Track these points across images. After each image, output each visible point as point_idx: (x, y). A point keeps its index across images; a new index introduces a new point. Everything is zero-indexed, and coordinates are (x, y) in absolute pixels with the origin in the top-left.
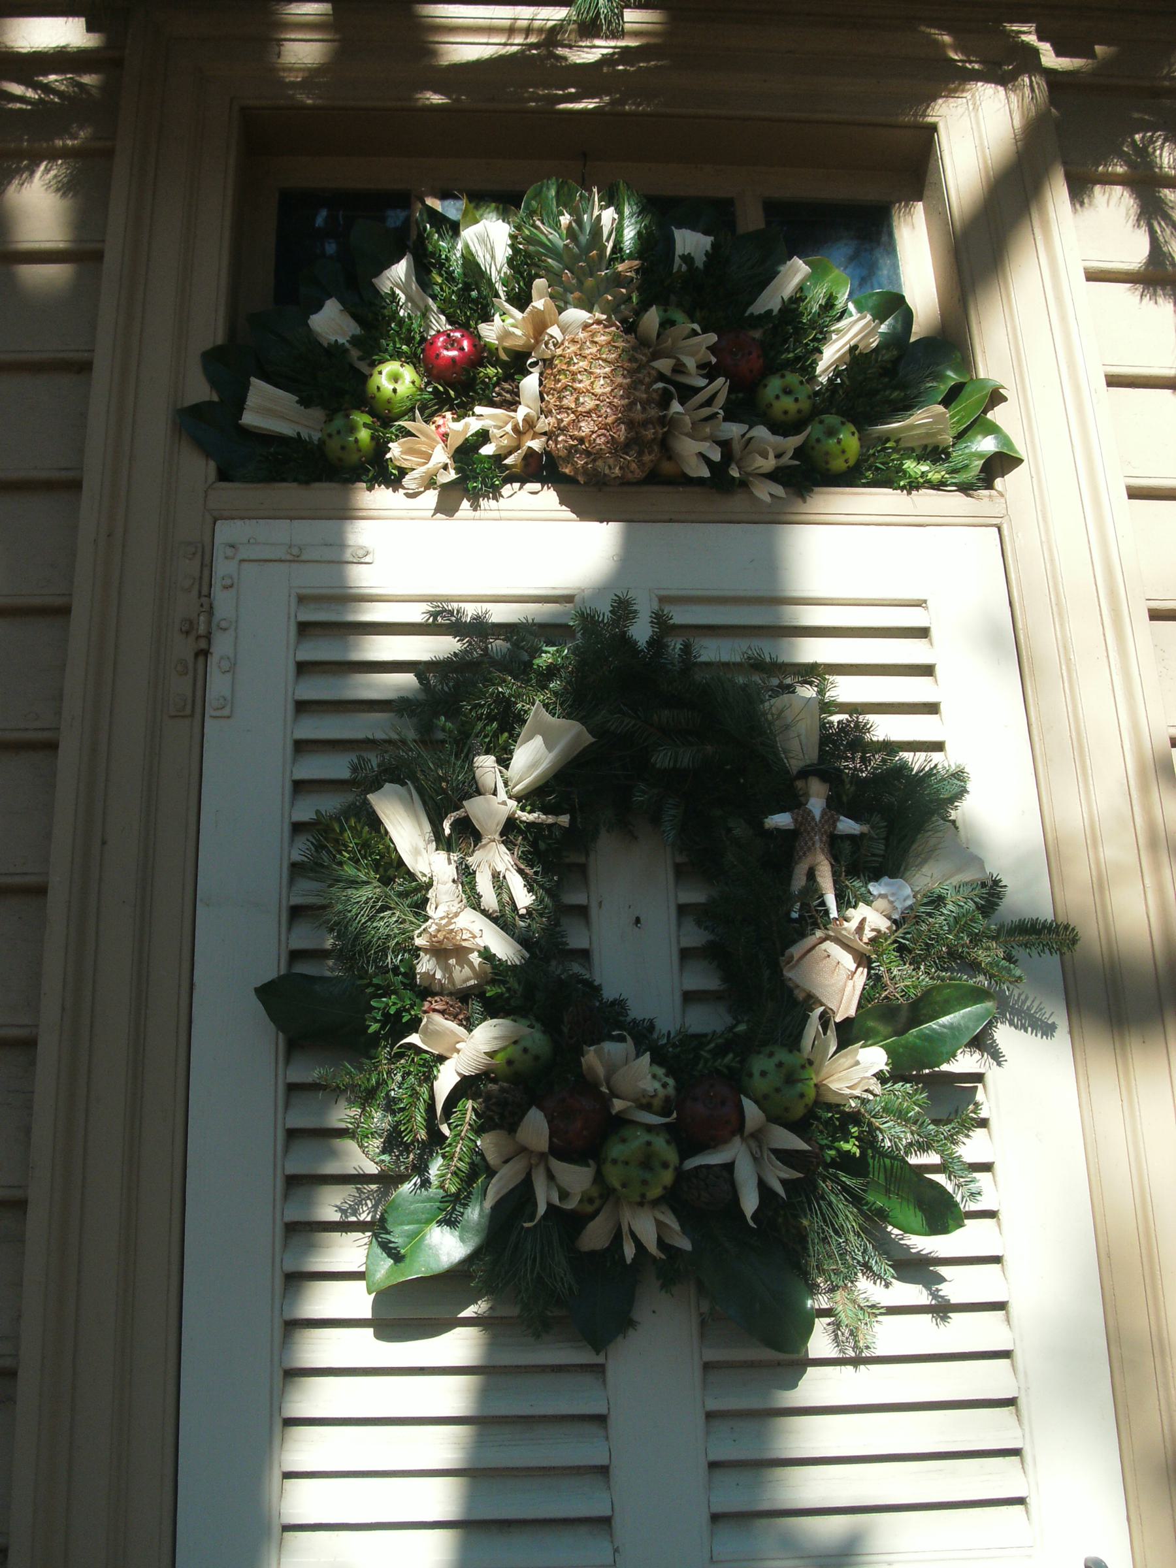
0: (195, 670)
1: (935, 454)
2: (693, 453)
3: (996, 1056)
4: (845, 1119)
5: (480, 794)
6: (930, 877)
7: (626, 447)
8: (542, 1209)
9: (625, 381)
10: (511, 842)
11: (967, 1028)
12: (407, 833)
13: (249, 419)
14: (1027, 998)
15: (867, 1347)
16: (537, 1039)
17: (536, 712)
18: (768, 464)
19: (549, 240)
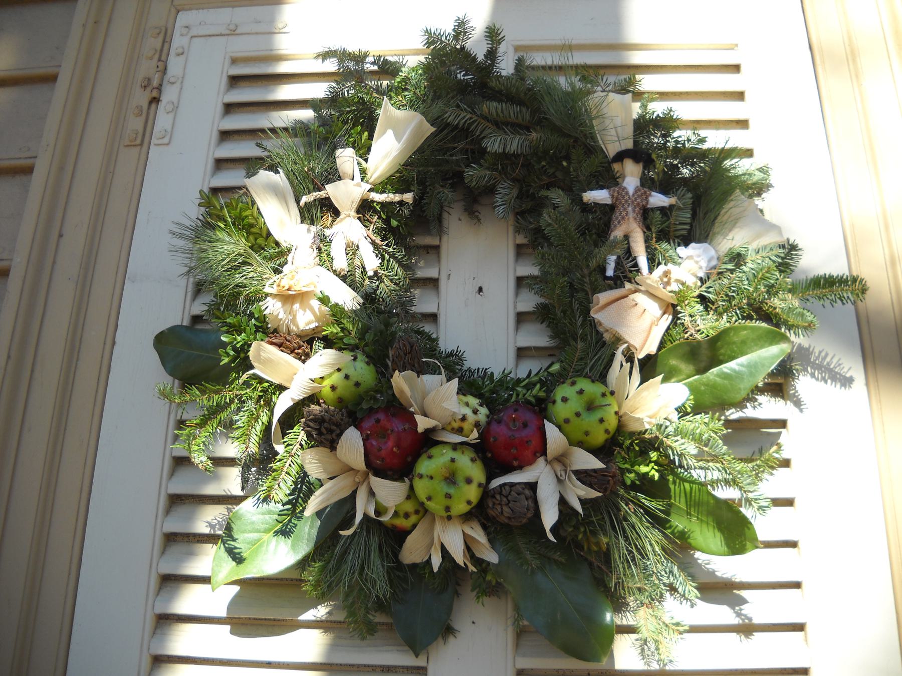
0: (148, 114)
3: (798, 403)
4: (647, 445)
6: (735, 239)
8: (359, 518)
10: (368, 220)
11: (763, 365)
12: (280, 217)
14: (827, 355)
15: (671, 661)
16: (363, 371)
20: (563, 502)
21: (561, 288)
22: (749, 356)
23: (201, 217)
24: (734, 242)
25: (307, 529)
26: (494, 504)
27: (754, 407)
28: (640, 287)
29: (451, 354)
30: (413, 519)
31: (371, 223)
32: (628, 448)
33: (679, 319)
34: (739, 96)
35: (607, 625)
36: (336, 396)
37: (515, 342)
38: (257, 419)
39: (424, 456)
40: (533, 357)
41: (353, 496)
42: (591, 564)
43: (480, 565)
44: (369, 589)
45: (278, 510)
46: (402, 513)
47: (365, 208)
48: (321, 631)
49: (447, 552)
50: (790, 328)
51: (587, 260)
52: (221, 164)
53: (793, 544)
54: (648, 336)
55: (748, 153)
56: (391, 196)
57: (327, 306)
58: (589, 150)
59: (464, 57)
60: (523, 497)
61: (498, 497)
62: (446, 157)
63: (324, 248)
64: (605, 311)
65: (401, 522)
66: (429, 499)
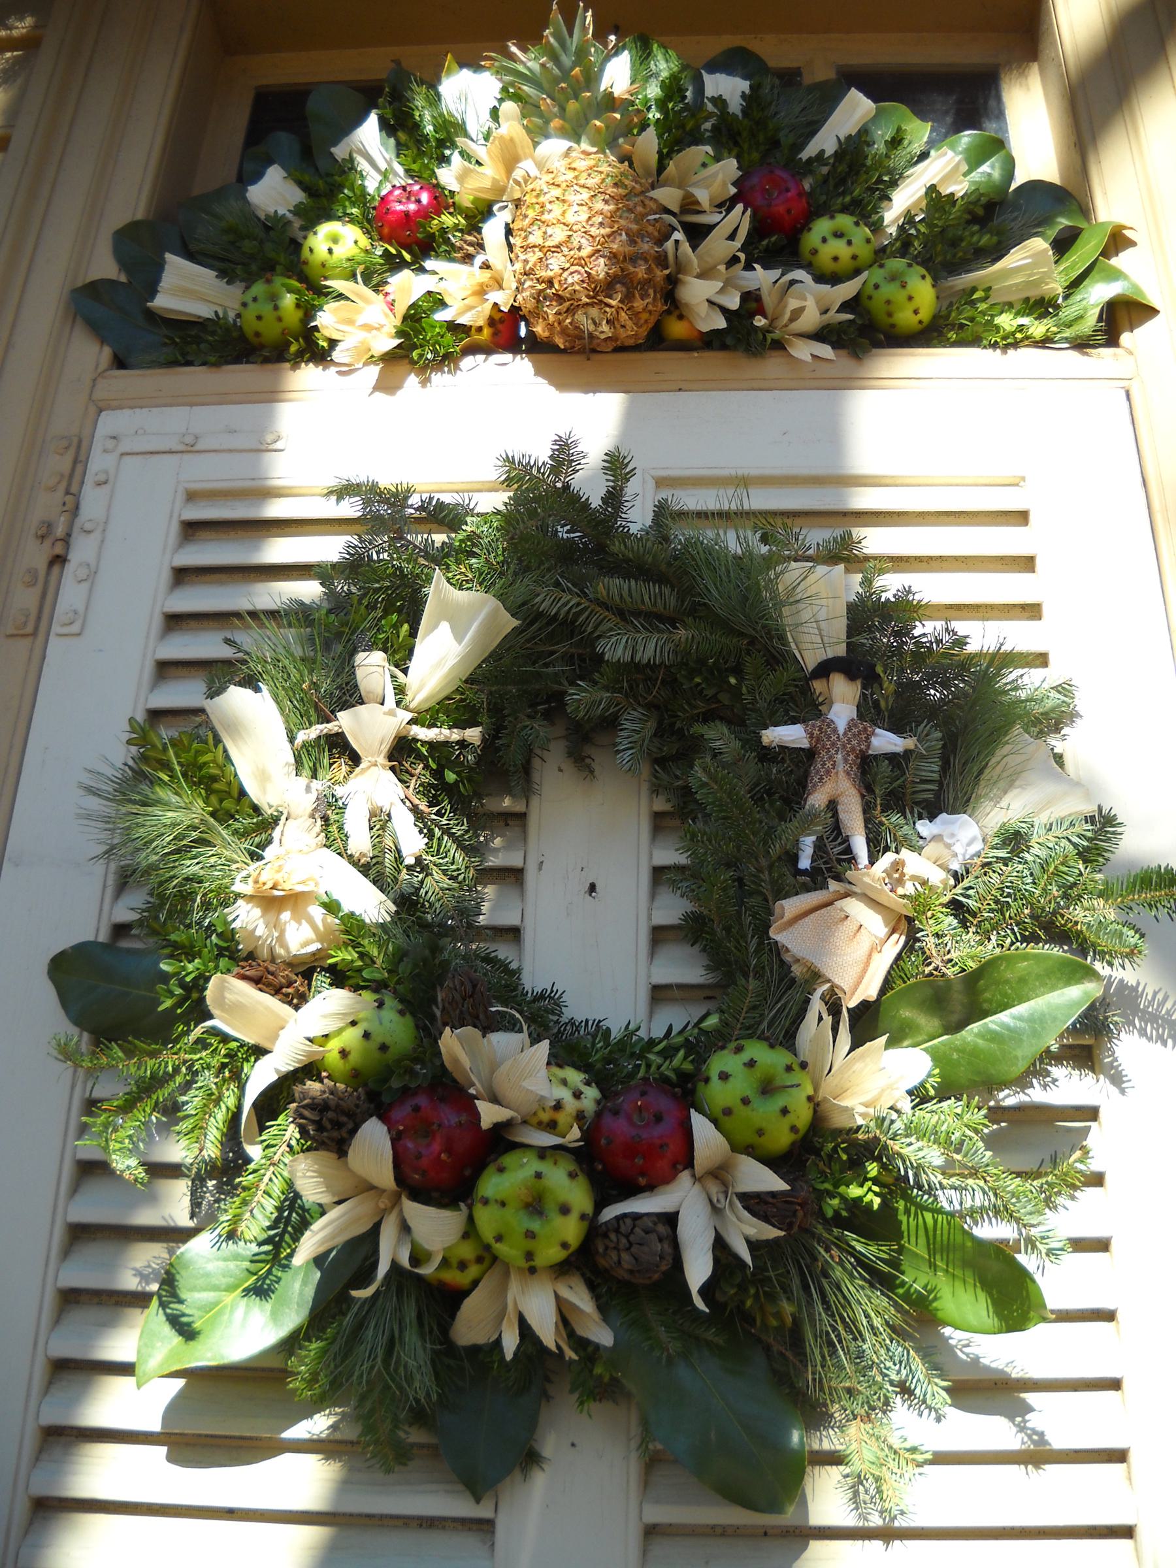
1: (1042, 307)
2: (706, 297)
3: (1117, 1079)
4: (861, 1151)
5: (362, 703)
7: (609, 286)
8: (383, 1269)
9: (607, 208)
10: (407, 772)
11: (1055, 1019)
13: (163, 301)
14: (1166, 998)
15: (902, 1513)
16: (395, 1027)
17: (440, 591)
18: (811, 319)
19: (529, 69)
20: (720, 1245)
21: (724, 889)
22: (1032, 1003)
23: (131, 763)
24: (1010, 814)
25: (297, 1285)
26: (607, 1248)
27: (1045, 1086)
28: (854, 889)
29: (541, 996)
30: (473, 1271)
31: (412, 776)
32: (830, 1157)
33: (919, 940)
34: (1027, 564)
35: (793, 1450)
36: (348, 1067)
37: (649, 976)
38: (218, 1101)
39: (491, 1169)
40: (673, 1000)
41: (374, 1233)
42: (767, 1349)
43: (585, 1349)
44: (400, 1388)
45: (249, 1253)
46: (454, 1262)
47: (402, 752)
48: (320, 1456)
49: (529, 1328)
50: (1102, 955)
51: (765, 843)
52: (166, 669)
53: (1108, 1316)
54: (865, 971)
55: (1042, 660)
56: (446, 732)
57: (337, 917)
58: (774, 657)
59: (568, 501)
60: (653, 1237)
61: (613, 1236)
62: (537, 668)
63: (333, 817)
64: (794, 929)
65: (453, 1277)
66: (499, 1238)
